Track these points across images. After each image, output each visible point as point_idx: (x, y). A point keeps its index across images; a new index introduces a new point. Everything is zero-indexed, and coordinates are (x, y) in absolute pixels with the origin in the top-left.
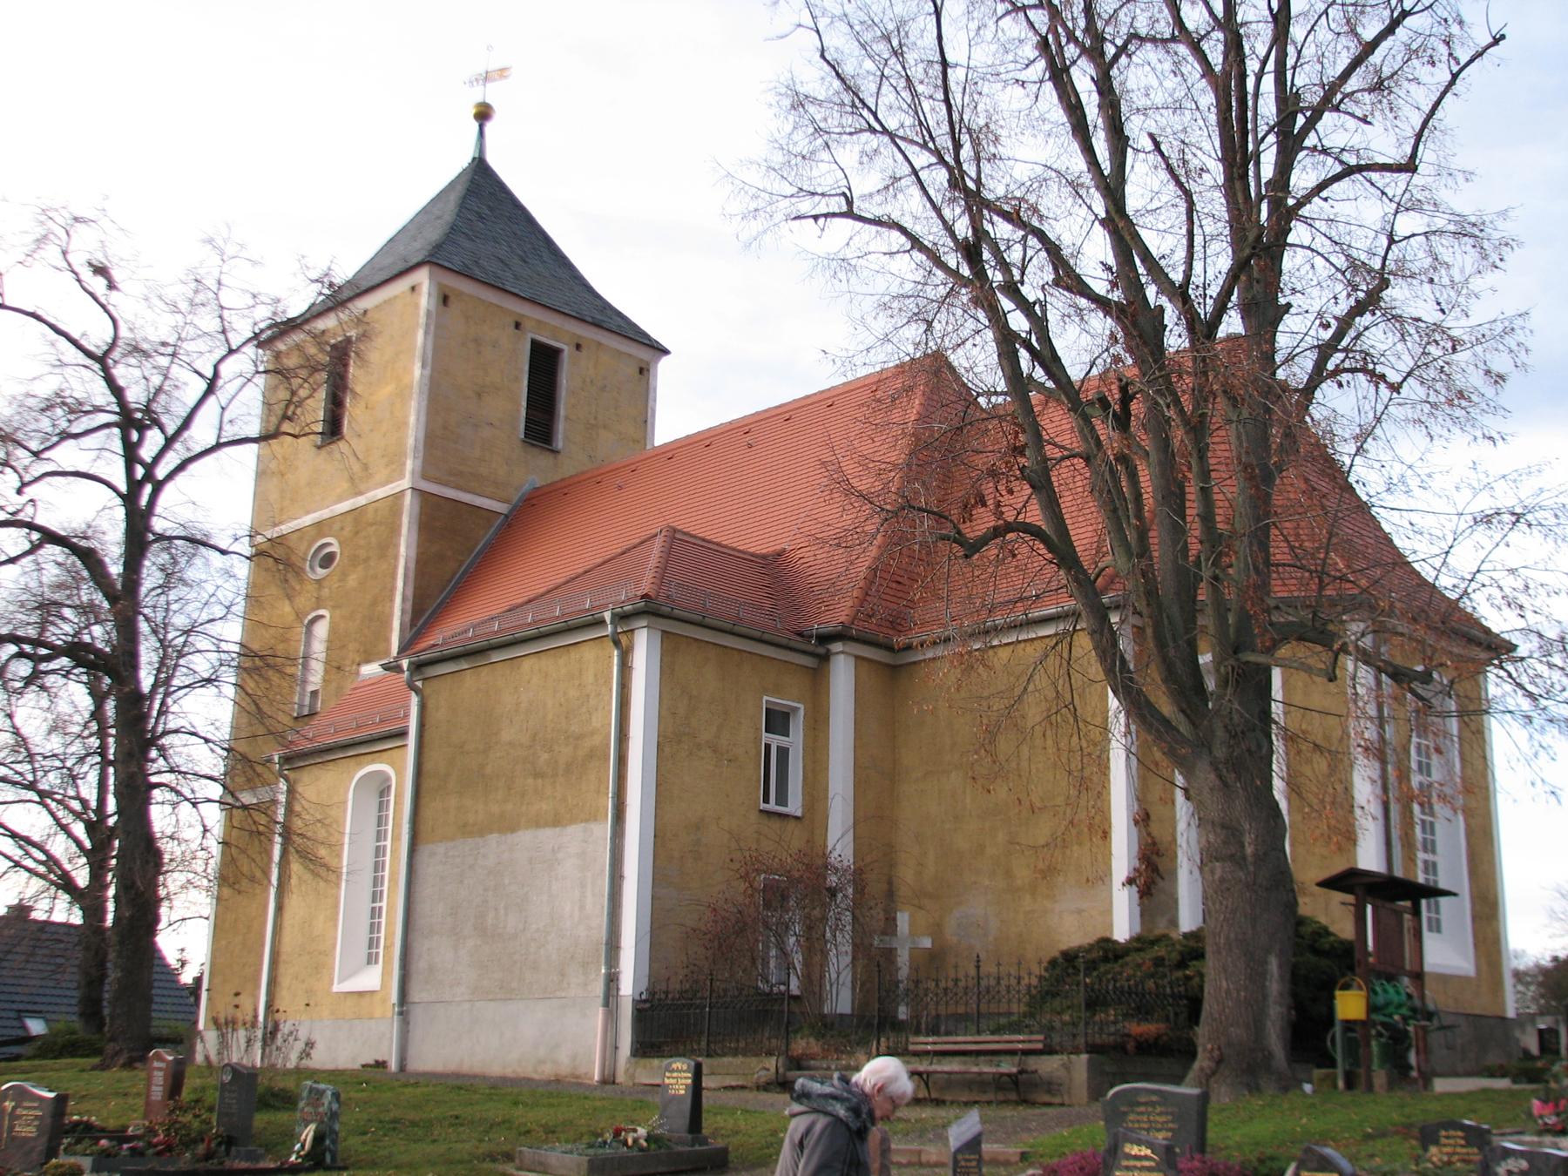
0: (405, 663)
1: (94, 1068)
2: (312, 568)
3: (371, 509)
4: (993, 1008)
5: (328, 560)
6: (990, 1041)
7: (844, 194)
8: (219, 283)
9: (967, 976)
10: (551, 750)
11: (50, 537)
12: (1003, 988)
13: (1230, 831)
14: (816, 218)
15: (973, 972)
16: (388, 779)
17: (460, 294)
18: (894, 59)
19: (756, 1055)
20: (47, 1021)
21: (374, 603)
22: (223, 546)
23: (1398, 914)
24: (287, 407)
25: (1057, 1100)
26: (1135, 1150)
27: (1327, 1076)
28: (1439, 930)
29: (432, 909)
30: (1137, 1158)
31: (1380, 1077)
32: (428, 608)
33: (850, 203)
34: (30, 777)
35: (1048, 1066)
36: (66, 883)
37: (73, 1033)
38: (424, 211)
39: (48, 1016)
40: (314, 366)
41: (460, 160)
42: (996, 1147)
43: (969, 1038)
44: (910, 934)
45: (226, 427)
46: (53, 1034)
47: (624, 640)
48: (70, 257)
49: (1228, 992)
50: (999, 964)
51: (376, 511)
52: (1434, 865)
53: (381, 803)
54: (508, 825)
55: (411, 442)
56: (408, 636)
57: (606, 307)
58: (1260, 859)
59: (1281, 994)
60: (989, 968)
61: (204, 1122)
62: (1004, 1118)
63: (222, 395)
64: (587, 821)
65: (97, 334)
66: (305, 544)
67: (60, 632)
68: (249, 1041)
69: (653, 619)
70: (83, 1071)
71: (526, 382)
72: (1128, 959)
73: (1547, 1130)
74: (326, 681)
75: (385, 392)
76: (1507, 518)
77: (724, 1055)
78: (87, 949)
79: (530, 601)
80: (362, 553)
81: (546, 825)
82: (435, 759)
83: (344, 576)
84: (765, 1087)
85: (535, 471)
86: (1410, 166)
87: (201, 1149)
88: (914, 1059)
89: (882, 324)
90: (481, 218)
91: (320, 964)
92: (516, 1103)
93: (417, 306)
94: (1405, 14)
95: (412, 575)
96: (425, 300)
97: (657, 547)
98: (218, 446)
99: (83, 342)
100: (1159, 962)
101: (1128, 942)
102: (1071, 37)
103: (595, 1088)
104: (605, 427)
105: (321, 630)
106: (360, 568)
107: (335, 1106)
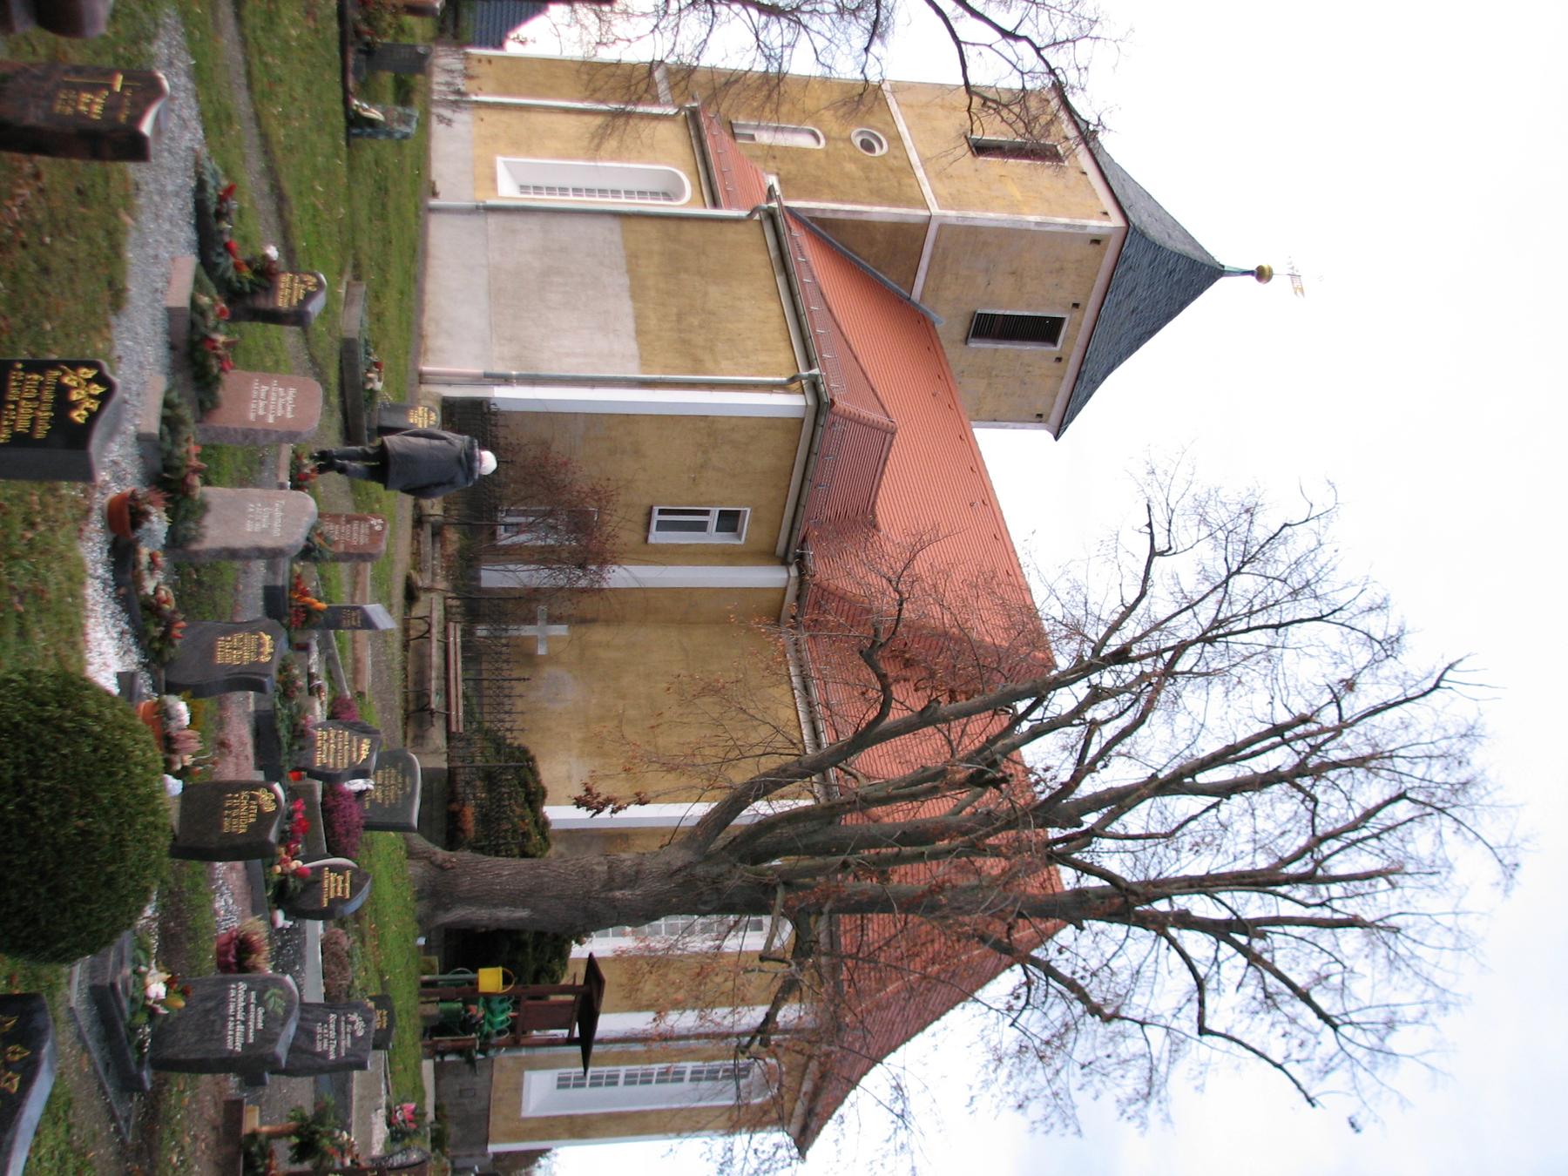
0: (774, 204)
3: (913, 181)
4: (486, 709)
6: (458, 688)
10: (701, 327)
14: (1150, 525)
17: (1102, 256)
21: (831, 186)
22: (872, 49)
24: (994, 101)
25: (409, 742)
26: (365, 747)
27: (433, 967)
28: (559, 1087)
29: (565, 231)
30: (359, 749)
31: (433, 1009)
33: (1162, 554)
35: (437, 736)
38: (1176, 224)
40: (1035, 128)
42: (369, 573)
44: (547, 636)
47: (795, 386)
54: (637, 292)
55: (971, 214)
56: (802, 215)
57: (1095, 384)
58: (612, 903)
60: (519, 688)
66: (880, 126)
68: (451, 71)
69: (813, 411)
71: (1026, 313)
73: (390, 1113)
75: (1014, 191)
76: (898, 1108)
79: (830, 310)
80: (873, 175)
82: (691, 231)
83: (855, 160)
85: (949, 323)
86: (1203, 1030)
87: (364, 27)
89: (1062, 587)
91: (519, 145)
92: (402, 293)
93: (1090, 217)
94: (1335, 1027)
97: (876, 416)
100: (526, 835)
101: (543, 815)
102: (1315, 749)
104: (989, 384)
107: (397, 135)
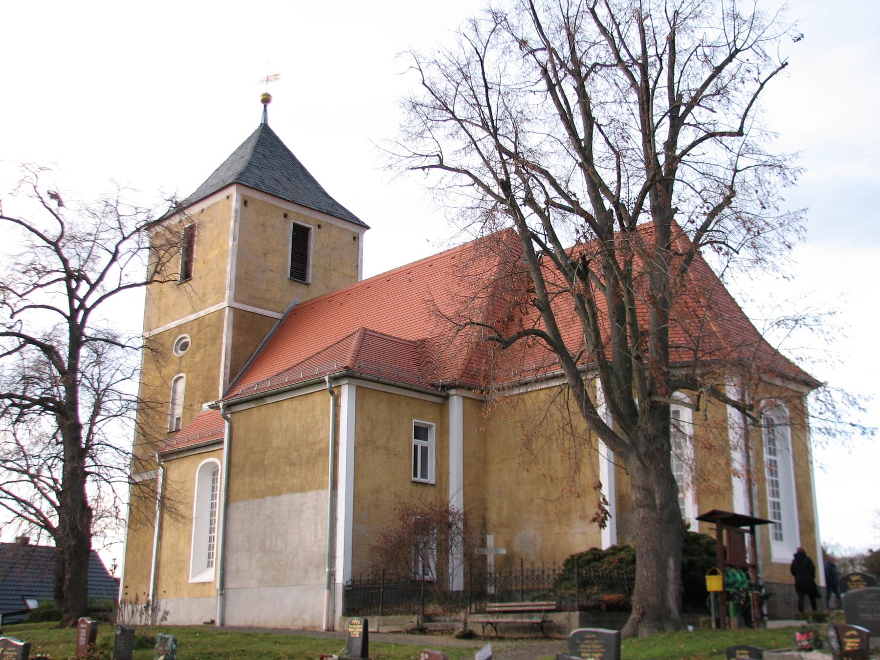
0: (221, 405)
1: (57, 627)
2: (176, 351)
3: (207, 318)
4: (541, 587)
5: (185, 346)
6: (528, 605)
7: (438, 155)
8: (117, 202)
9: (559, 568)
10: (299, 451)
11: (29, 340)
12: (545, 576)
13: (648, 492)
14: (423, 168)
15: (519, 568)
16: (217, 466)
17: (254, 199)
18: (464, 82)
19: (407, 614)
20: (38, 601)
21: (210, 369)
22: (123, 343)
23: (742, 533)
24: (157, 267)
25: (563, 636)
27: (707, 621)
28: (781, 539)
29: (236, 538)
31: (734, 621)
32: (239, 371)
33: (441, 160)
34: (26, 468)
35: (559, 618)
36: (47, 526)
37: (52, 607)
38: (234, 154)
39: (39, 598)
40: (174, 241)
41: (254, 125)
43: (517, 604)
44: (494, 548)
45: (123, 278)
46: (41, 608)
47: (336, 391)
48: (37, 189)
49: (647, 578)
50: (543, 563)
51: (210, 319)
52: (778, 504)
53: (214, 479)
54: (276, 492)
55: (228, 281)
56: (228, 387)
57: (335, 204)
58: (664, 506)
59: (675, 578)
60: (527, 565)
61: (105, 656)
62: (531, 647)
63: (121, 261)
64: (318, 489)
65: (53, 230)
67: (36, 392)
70: (51, 629)
72: (606, 559)
74: (184, 413)
77: (391, 614)
78: (58, 561)
80: (203, 342)
81: (297, 491)
82: (238, 457)
83: (193, 355)
84: (411, 632)
85: (297, 295)
86: (740, 133)
88: (489, 615)
90: (265, 157)
91: (182, 567)
92: (276, 643)
93: (230, 207)
95: (229, 354)
96: (234, 203)
97: (355, 340)
98: (119, 289)
99: (45, 235)
100: (621, 561)
101: (608, 550)
102: (563, 65)
103: (321, 633)
105: (181, 386)
106: (202, 350)
107: (174, 646)
